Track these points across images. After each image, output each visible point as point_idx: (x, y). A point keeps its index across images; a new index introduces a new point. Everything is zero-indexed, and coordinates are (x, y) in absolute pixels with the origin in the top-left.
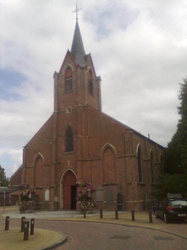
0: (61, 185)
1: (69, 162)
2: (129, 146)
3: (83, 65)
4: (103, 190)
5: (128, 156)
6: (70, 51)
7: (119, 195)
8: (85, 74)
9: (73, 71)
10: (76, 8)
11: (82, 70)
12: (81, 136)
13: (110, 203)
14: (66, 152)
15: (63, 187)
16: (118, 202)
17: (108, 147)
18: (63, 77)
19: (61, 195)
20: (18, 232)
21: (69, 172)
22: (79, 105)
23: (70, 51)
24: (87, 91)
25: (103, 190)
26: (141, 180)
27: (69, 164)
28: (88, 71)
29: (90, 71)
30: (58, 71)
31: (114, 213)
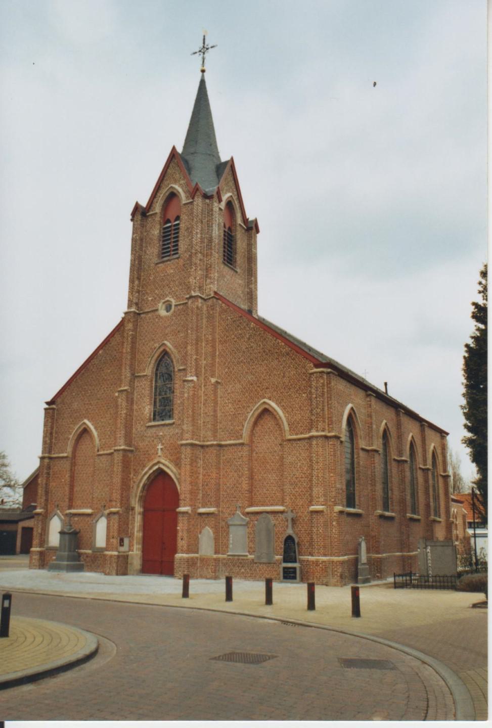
0: (138, 509)
1: (160, 447)
2: (323, 410)
3: (211, 189)
4: (247, 525)
5: (317, 437)
6: (180, 150)
7: (289, 539)
8: (216, 209)
9: (184, 202)
10: (202, 45)
11: (207, 201)
12: (195, 378)
13: (264, 560)
14: (154, 419)
15: (145, 515)
16: (285, 560)
17: (266, 412)
18: (158, 218)
19: (138, 534)
20: (469, 607)
21: (161, 474)
22: (193, 294)
23: (180, 150)
24: (217, 256)
25: (247, 525)
26: (351, 502)
27: (160, 453)
28: (223, 205)
29: (229, 204)
30: (144, 203)
31: (261, 586)
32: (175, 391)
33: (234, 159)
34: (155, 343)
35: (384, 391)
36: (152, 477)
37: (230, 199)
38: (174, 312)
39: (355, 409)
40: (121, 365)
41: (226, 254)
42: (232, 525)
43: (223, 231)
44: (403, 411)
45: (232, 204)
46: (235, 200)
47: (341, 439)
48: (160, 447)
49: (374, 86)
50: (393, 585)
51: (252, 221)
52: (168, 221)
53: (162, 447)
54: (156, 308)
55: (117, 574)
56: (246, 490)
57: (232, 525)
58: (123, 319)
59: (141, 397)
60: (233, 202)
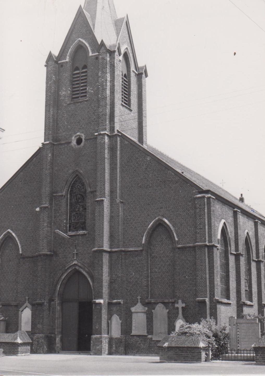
17: (160, 224)
30: (56, 53)
32: (87, 208)
33: (128, 14)
37: (126, 50)
39: (226, 223)
43: (121, 78)
44: (260, 222)
45: (127, 54)
46: (130, 54)
47: (218, 248)
49: (235, 55)
51: (142, 68)
52: (77, 69)
54: (70, 141)
56: (145, 286)
58: (40, 149)
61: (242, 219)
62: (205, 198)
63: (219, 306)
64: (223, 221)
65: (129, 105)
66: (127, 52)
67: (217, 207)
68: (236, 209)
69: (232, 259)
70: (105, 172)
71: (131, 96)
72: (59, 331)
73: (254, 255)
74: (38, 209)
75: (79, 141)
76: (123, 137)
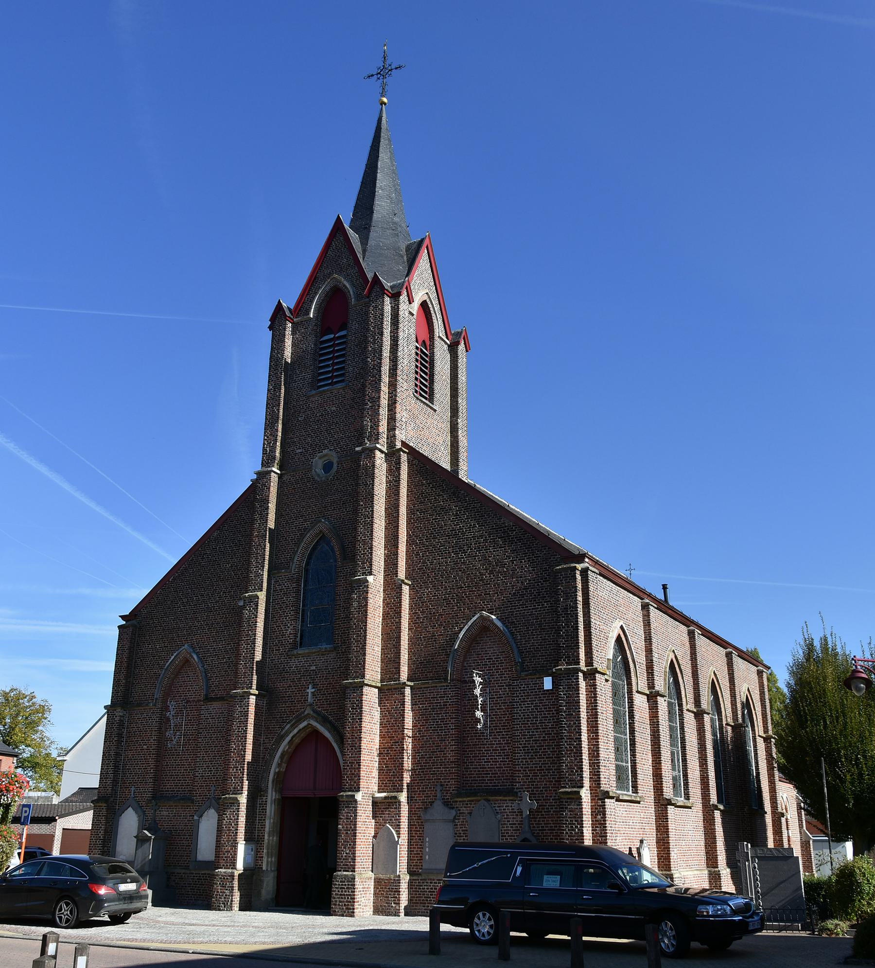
1: (310, 690)
28: (415, 307)
34: (305, 521)
35: (663, 599)
36: (297, 741)
37: (426, 298)
38: (337, 472)
39: (624, 627)
40: (249, 556)
41: (419, 359)
42: (367, 685)
48: (310, 690)
50: (426, 948)
53: (313, 690)
55: (245, 906)
57: (367, 685)
59: (281, 608)
60: (429, 303)
61: (702, 642)
62: (578, 572)
63: (671, 809)
64: (618, 624)
65: (431, 399)
66: (428, 300)
67: (600, 589)
68: (691, 628)
69: (690, 720)
70: (373, 522)
71: (436, 384)
72: (272, 861)
73: (691, 700)
74: (548, 683)
75: (327, 467)
76: (415, 456)
